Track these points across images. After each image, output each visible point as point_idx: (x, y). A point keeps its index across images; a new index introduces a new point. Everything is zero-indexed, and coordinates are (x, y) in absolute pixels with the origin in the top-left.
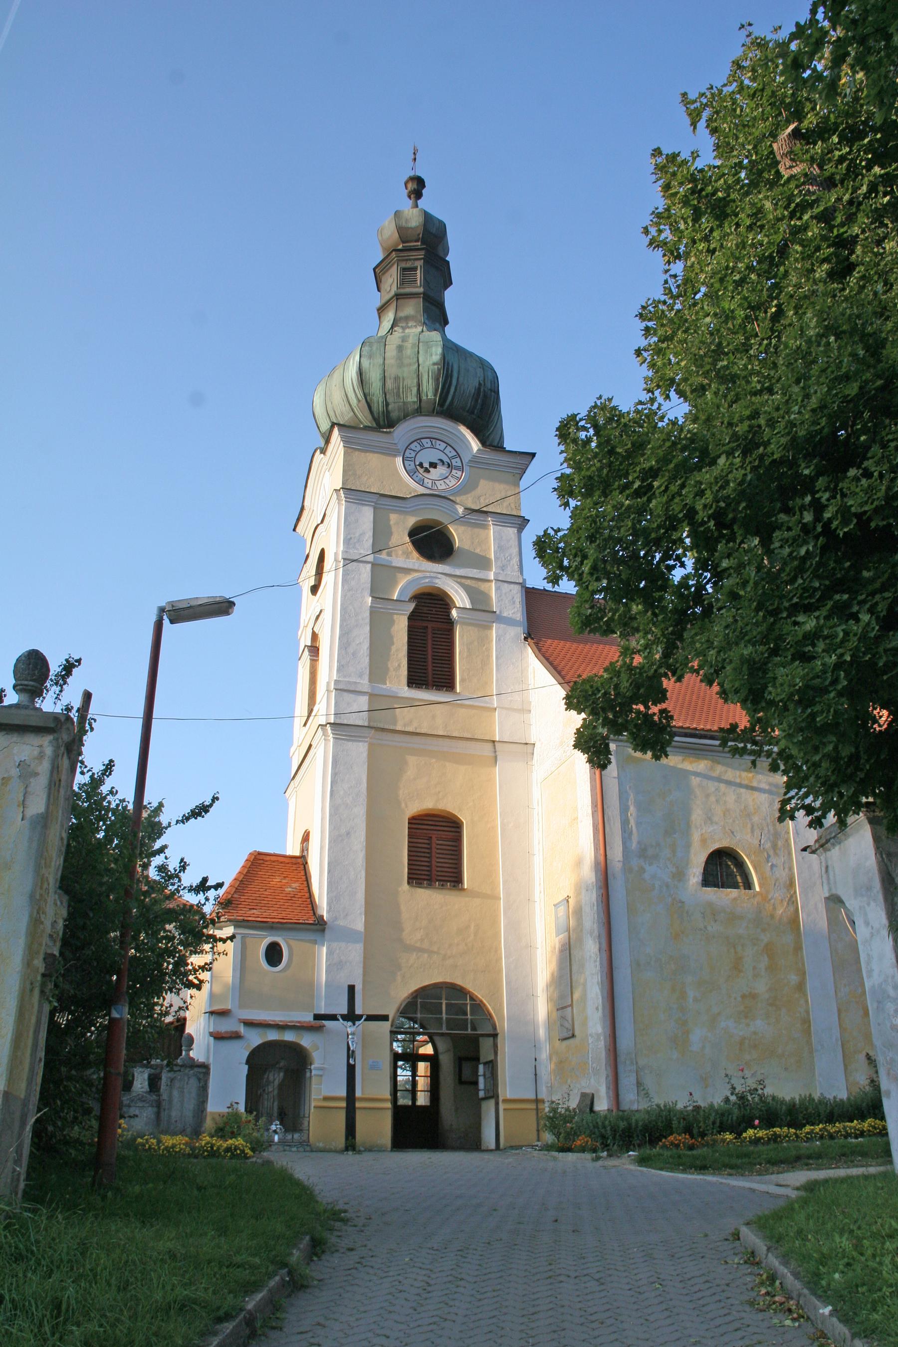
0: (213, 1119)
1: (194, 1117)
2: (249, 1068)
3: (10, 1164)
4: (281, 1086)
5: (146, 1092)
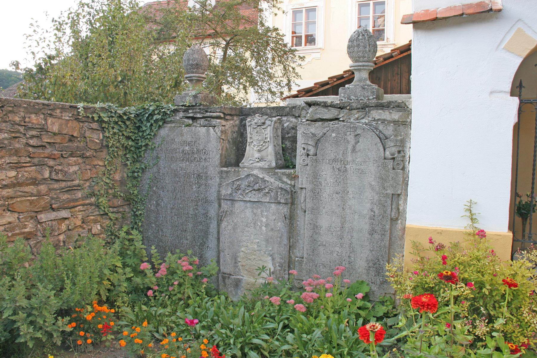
0: (416, 246)
1: (372, 232)
2: (520, 103)
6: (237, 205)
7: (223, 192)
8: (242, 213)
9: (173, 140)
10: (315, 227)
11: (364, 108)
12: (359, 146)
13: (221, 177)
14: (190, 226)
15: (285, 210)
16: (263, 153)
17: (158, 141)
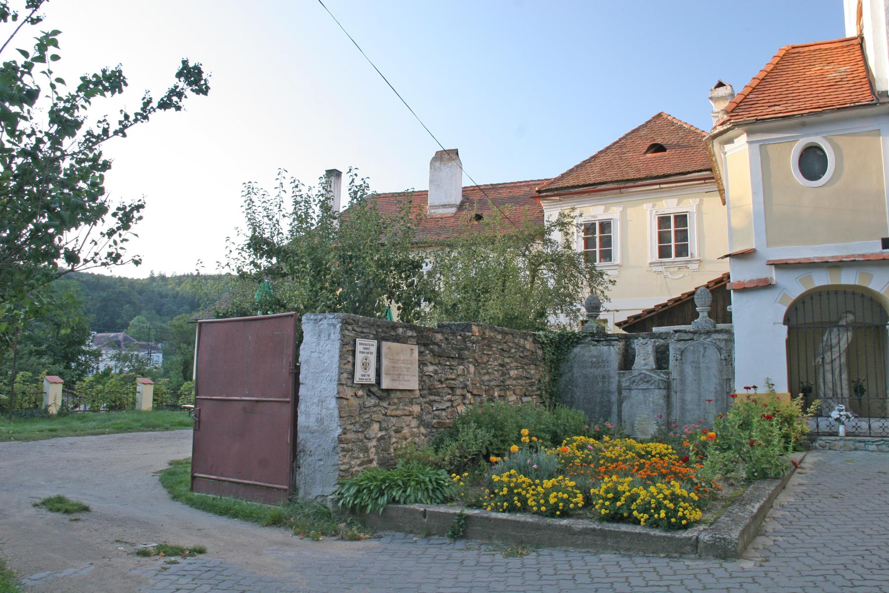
2: (789, 332)
3: (638, 529)
4: (849, 351)
5: (652, 370)
6: (633, 392)
7: (624, 385)
8: (636, 396)
9: (583, 355)
10: (683, 401)
11: (708, 333)
12: (707, 353)
13: (619, 377)
14: (598, 409)
15: (664, 392)
16: (647, 361)
17: (572, 356)
